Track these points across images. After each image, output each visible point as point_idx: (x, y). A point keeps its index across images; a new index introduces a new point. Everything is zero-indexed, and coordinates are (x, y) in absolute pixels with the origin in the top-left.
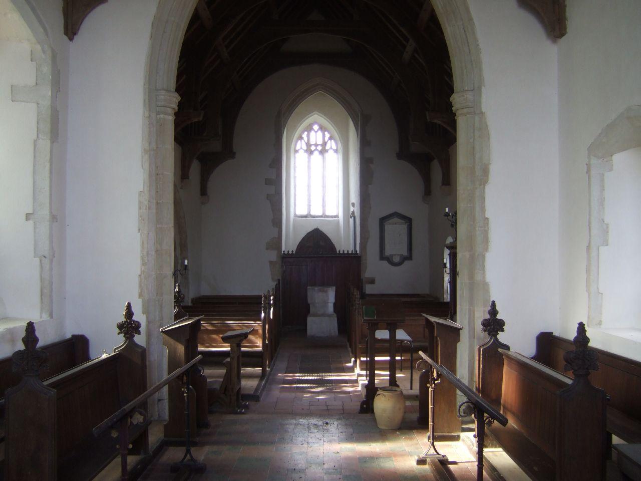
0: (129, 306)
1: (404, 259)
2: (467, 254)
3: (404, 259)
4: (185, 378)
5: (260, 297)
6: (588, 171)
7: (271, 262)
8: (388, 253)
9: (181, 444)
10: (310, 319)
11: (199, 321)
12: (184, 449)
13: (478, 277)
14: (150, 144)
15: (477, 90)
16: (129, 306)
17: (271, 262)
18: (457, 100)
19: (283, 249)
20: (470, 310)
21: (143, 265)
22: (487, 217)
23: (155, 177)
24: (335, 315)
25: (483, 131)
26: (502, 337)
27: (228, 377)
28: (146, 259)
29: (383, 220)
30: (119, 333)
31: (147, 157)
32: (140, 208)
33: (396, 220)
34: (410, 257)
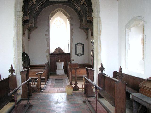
0: (12, 65)
1: (82, 55)
2: (96, 52)
3: (82, 55)
4: (28, 83)
5: (44, 65)
6: (125, 32)
7: (47, 56)
8: (77, 53)
9: (27, 100)
10: (57, 70)
11: (29, 69)
12: (27, 101)
13: (99, 58)
14: (16, 25)
15: (98, 12)
16: (12, 65)
17: (47, 56)
18: (94, 14)
19: (50, 52)
20: (97, 66)
21: (15, 56)
22: (101, 43)
23: (17, 34)
24: (64, 69)
25: (99, 22)
26: (104, 72)
27: (38, 84)
28: (15, 54)
29: (76, 45)
30: (9, 72)
31: (15, 28)
32: (14, 41)
33: (79, 45)
34: (83, 54)
